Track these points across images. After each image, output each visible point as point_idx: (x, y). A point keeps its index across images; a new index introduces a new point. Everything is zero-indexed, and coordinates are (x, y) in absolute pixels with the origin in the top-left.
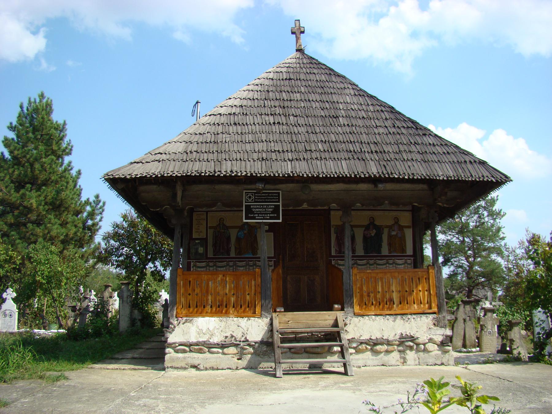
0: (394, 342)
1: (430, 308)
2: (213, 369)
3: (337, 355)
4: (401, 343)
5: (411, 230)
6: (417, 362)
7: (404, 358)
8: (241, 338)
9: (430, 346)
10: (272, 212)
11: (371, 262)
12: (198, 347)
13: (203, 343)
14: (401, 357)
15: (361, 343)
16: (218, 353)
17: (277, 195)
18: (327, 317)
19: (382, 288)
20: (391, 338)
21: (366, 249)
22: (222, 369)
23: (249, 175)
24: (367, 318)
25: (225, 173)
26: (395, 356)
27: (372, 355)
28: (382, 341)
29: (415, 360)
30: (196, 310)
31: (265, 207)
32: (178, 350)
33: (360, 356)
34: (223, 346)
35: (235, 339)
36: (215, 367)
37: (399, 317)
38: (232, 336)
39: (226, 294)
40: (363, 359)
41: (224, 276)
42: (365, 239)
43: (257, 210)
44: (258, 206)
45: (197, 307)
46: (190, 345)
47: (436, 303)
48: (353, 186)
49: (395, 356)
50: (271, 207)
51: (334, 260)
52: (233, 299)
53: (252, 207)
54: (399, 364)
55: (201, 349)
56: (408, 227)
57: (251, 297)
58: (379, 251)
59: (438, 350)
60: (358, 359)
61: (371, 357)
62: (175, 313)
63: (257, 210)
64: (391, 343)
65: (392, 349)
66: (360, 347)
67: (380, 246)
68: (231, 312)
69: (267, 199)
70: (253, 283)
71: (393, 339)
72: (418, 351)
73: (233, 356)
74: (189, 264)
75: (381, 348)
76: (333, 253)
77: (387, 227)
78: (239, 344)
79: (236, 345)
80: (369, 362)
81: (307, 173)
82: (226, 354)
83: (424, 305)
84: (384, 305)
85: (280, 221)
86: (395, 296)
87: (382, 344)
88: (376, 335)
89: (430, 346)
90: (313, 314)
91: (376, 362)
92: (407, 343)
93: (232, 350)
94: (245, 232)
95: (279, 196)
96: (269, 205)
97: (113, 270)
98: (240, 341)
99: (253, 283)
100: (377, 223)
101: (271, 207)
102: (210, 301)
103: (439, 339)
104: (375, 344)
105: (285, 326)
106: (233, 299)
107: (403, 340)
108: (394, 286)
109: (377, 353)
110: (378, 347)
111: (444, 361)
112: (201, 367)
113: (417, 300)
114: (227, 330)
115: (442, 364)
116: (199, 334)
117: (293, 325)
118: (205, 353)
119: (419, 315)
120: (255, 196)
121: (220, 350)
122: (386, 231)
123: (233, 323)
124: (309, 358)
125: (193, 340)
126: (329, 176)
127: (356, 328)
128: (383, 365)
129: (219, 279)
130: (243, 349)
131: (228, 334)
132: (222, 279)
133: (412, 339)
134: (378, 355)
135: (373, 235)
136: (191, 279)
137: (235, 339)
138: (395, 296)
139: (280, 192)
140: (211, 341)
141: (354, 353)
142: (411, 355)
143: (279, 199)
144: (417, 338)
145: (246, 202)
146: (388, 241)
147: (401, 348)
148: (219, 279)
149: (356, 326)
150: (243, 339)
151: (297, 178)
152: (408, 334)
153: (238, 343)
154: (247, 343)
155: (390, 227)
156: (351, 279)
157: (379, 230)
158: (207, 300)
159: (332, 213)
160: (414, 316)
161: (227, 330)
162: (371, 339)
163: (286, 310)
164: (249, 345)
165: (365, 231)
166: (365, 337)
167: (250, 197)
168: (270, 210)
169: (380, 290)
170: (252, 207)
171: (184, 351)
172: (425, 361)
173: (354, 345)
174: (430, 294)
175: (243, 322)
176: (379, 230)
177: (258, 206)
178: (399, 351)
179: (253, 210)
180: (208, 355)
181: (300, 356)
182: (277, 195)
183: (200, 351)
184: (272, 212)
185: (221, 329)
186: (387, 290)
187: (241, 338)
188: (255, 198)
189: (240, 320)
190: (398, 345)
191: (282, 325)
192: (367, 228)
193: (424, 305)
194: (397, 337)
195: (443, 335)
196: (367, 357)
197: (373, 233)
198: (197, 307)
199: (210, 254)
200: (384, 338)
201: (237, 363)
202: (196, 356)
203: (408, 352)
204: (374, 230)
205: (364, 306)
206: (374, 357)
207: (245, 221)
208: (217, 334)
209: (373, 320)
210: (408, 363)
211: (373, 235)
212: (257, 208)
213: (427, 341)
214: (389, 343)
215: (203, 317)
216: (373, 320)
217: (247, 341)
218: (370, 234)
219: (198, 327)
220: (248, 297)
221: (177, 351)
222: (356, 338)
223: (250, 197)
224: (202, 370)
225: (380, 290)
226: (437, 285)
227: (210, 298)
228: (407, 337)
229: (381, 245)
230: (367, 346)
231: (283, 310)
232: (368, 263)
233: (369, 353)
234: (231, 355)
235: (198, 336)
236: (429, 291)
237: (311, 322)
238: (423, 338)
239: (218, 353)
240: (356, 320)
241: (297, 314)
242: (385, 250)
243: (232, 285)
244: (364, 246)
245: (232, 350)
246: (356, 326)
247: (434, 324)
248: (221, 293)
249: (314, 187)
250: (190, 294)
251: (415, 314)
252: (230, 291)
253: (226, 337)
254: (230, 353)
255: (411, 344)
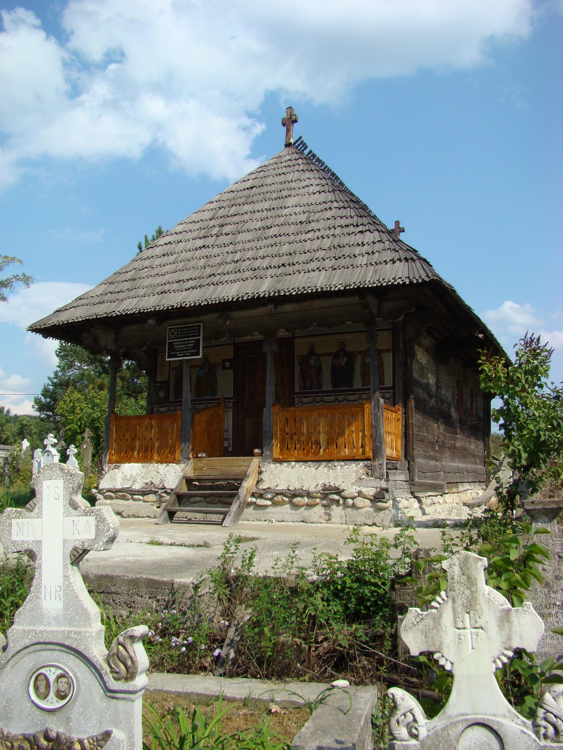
0: (315, 494)
1: (364, 453)
2: (134, 516)
3: (252, 507)
4: (325, 496)
5: (390, 355)
6: (343, 521)
7: (329, 515)
8: (159, 485)
9: (359, 501)
10: (193, 348)
11: (341, 398)
12: (122, 494)
13: (126, 490)
14: (325, 513)
15: (278, 494)
16: (139, 500)
17: (198, 328)
18: (242, 463)
19: (308, 429)
20: (312, 489)
21: (335, 383)
22: (142, 517)
23: (320, 290)
24: (285, 464)
25: (359, 284)
26: (319, 510)
27: (291, 509)
28: (301, 492)
29: (341, 518)
30: (125, 456)
31: (186, 342)
32: (106, 496)
33: (278, 509)
34: (143, 493)
35: (154, 486)
36: (136, 515)
37: (324, 464)
38: (152, 483)
39: (152, 439)
40: (280, 512)
41: (150, 420)
42: (334, 370)
43: (179, 346)
44: (179, 343)
45: (126, 453)
46: (116, 491)
47: (371, 447)
48: (305, 305)
49: (319, 510)
50: (192, 342)
51: (297, 397)
52: (157, 444)
53: (174, 344)
54: (323, 521)
55: (124, 496)
56: (387, 351)
57: (172, 442)
58: (351, 385)
59: (371, 507)
60: (275, 513)
61: (289, 511)
62: (107, 460)
63: (179, 346)
64: (311, 495)
65: (313, 503)
66: (276, 498)
67: (352, 377)
68: (155, 458)
69: (189, 333)
70: (175, 425)
71: (314, 490)
72: (346, 506)
73: (153, 503)
74: (152, 409)
75: (299, 502)
76: (297, 389)
77: (360, 352)
78: (158, 492)
79: (155, 493)
80: (287, 517)
81: (423, 277)
82: (146, 502)
83: (357, 449)
84: (310, 451)
85: (200, 357)
86: (323, 438)
87: (302, 496)
88: (295, 485)
89: (359, 501)
90: (228, 460)
91: (296, 518)
92: (331, 495)
93: (152, 497)
94: (206, 371)
95: (200, 329)
96: (189, 340)
97: (153, 422)
98: (159, 489)
99: (175, 425)
100: (349, 349)
101: (192, 342)
102: (137, 446)
103: (370, 491)
104: (295, 496)
105: (436, 499)
106: (157, 444)
107: (326, 492)
108: (321, 427)
109: (296, 506)
110: (297, 500)
111: (377, 521)
112: (124, 514)
113: (350, 443)
114: (147, 476)
115: (374, 524)
116: (124, 480)
117: (207, 472)
118: (128, 500)
119: (348, 463)
120: (178, 332)
121: (141, 497)
122: (359, 358)
123: (153, 469)
124: (224, 508)
125: (119, 486)
126: (415, 282)
127: (272, 476)
128: (303, 521)
129: (146, 423)
130: (161, 497)
131: (148, 481)
132: (148, 423)
133: (338, 491)
134: (298, 510)
135: (343, 364)
136: (122, 424)
137: (154, 486)
138: (323, 438)
139: (201, 324)
140: (133, 487)
141: (271, 505)
142: (336, 511)
143: (200, 332)
144: (343, 490)
145: (169, 339)
146: (361, 371)
147: (325, 502)
148: (146, 423)
149: (272, 473)
150: (161, 486)
151: (138, 315)
152: (332, 484)
153: (157, 490)
154: (165, 490)
155: (364, 353)
156: (272, 418)
157: (351, 357)
158: (135, 445)
159: (297, 341)
160: (342, 463)
161: (147, 476)
162: (289, 490)
163: (210, 455)
164: (165, 492)
165: (333, 360)
166: (282, 487)
167: (173, 334)
168: (191, 345)
169: (305, 431)
170: (174, 344)
171: (111, 498)
172: (352, 519)
173: (269, 496)
174: (364, 436)
175: (162, 468)
176: (351, 357)
177: (179, 343)
178: (324, 506)
179: (176, 347)
180: (131, 502)
181: (213, 505)
182: (198, 328)
183: (124, 498)
184: (193, 348)
185: (142, 475)
186: (312, 431)
187: (159, 485)
188: (178, 334)
189: (160, 466)
190: (322, 499)
191: (197, 471)
192: (336, 356)
193: (357, 449)
194: (320, 488)
195: (377, 488)
196: (285, 511)
197: (343, 361)
198: (126, 453)
199: (172, 399)
200: (304, 489)
201: (156, 511)
202: (120, 503)
203: (334, 507)
204: (345, 359)
205: (286, 451)
206: (293, 512)
207: (167, 360)
208: (139, 480)
209: (292, 467)
210: (333, 520)
211: (343, 364)
212: (179, 345)
213: (357, 494)
214: (309, 495)
215: (130, 462)
216: (292, 467)
217: (165, 488)
218: (340, 363)
219: (123, 473)
220: (170, 442)
221: (106, 498)
222: (272, 488)
223: (173, 334)
224: (126, 517)
225: (305, 431)
226: (374, 423)
227: (137, 443)
228: (331, 488)
229: (353, 376)
230: (284, 498)
231: (204, 455)
232: (314, 401)
233: (288, 506)
234: (150, 503)
235: (123, 482)
236: (363, 431)
237: (226, 468)
238: (351, 490)
239: (139, 500)
240: (273, 466)
241: (213, 460)
242: (357, 383)
243: (157, 430)
244: (332, 379)
245: (151, 497)
246: (272, 473)
247: (367, 474)
248: (148, 437)
249: (237, 314)
250: (121, 440)
251: (343, 460)
252: (154, 435)
253: (147, 483)
254: (149, 500)
255: (336, 497)
